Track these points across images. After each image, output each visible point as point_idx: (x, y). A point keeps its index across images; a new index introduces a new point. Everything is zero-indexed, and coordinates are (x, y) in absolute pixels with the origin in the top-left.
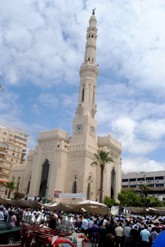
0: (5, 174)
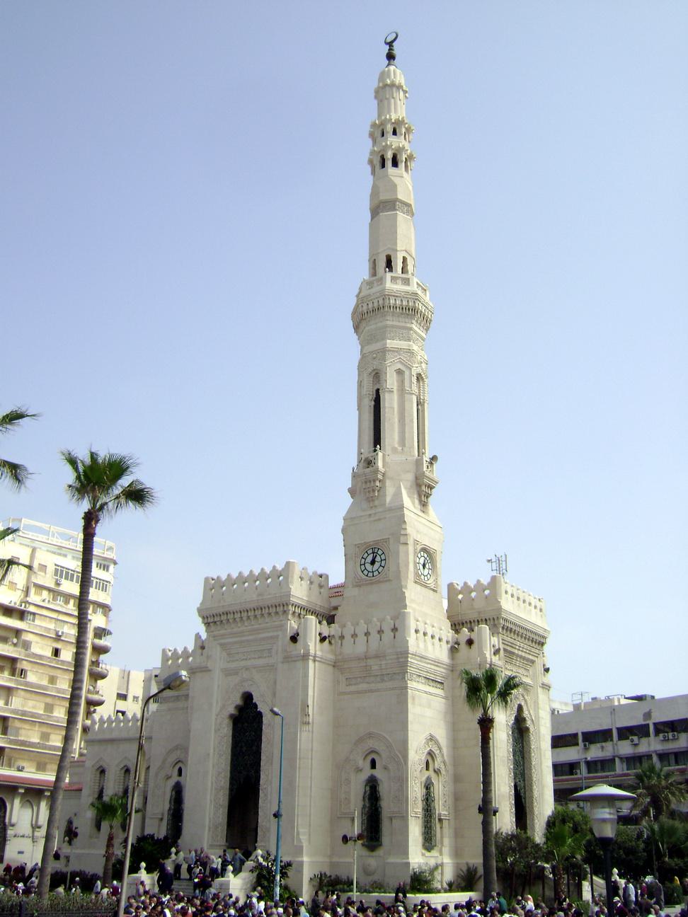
0: (23, 743)
